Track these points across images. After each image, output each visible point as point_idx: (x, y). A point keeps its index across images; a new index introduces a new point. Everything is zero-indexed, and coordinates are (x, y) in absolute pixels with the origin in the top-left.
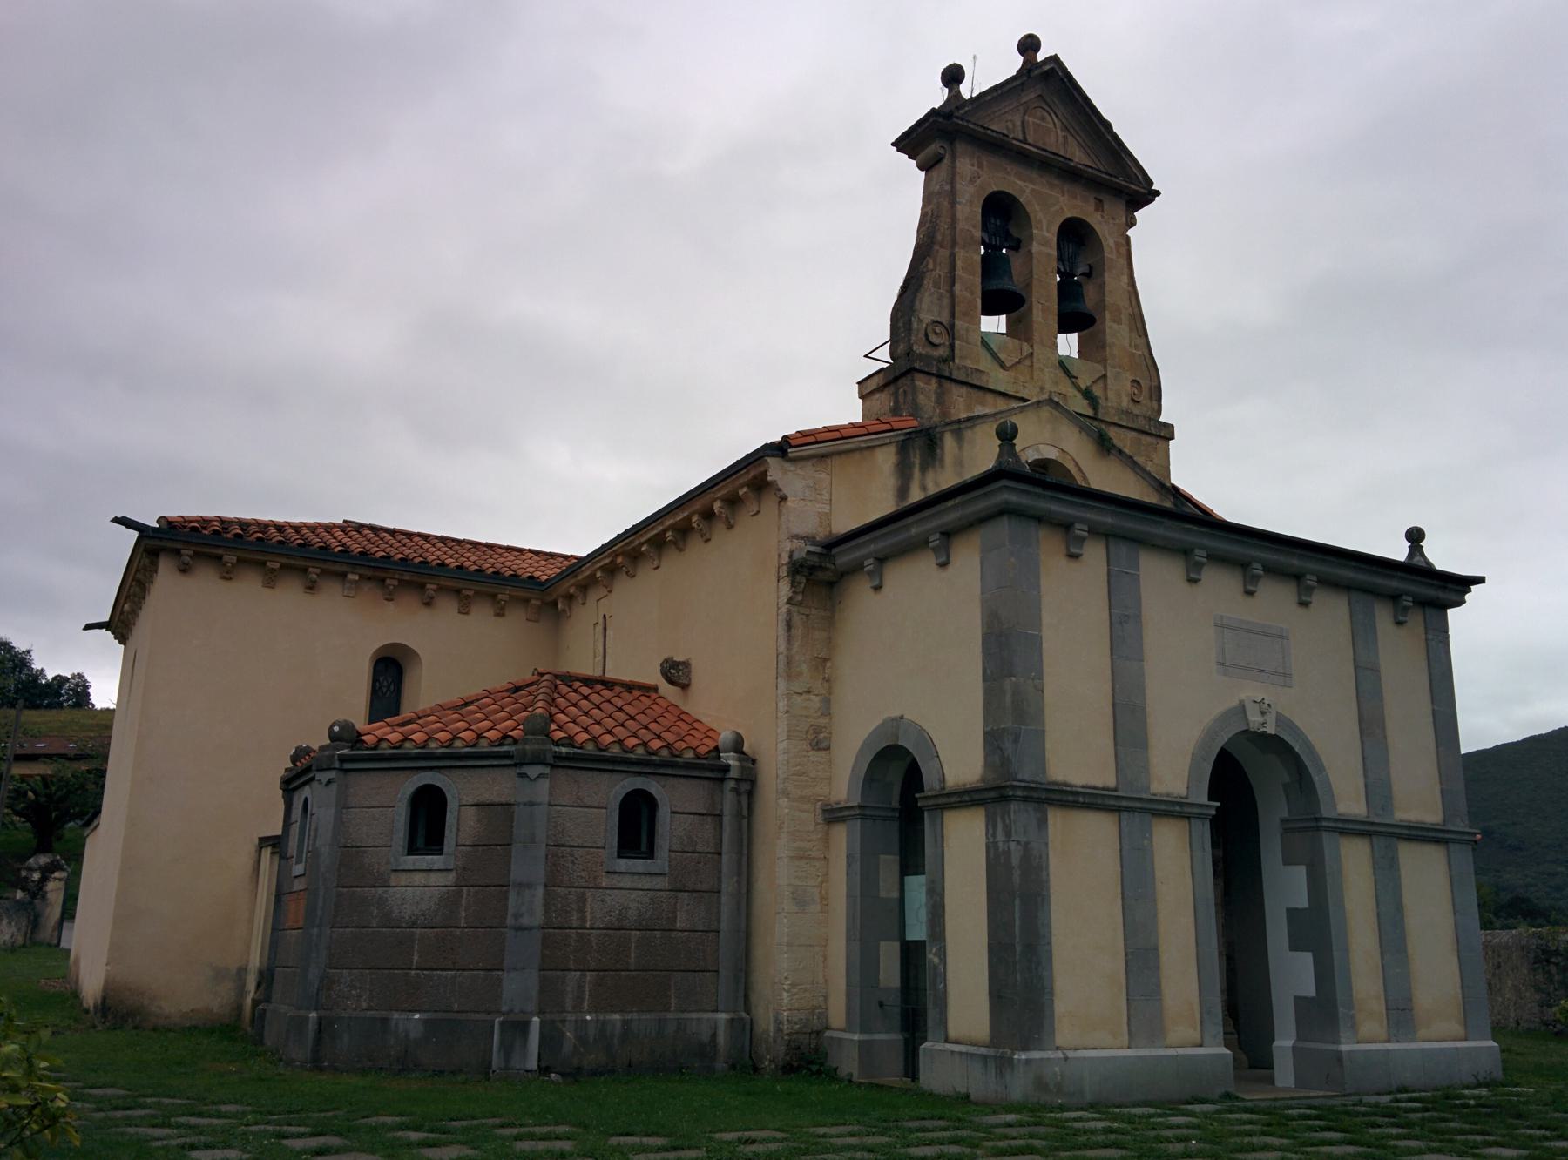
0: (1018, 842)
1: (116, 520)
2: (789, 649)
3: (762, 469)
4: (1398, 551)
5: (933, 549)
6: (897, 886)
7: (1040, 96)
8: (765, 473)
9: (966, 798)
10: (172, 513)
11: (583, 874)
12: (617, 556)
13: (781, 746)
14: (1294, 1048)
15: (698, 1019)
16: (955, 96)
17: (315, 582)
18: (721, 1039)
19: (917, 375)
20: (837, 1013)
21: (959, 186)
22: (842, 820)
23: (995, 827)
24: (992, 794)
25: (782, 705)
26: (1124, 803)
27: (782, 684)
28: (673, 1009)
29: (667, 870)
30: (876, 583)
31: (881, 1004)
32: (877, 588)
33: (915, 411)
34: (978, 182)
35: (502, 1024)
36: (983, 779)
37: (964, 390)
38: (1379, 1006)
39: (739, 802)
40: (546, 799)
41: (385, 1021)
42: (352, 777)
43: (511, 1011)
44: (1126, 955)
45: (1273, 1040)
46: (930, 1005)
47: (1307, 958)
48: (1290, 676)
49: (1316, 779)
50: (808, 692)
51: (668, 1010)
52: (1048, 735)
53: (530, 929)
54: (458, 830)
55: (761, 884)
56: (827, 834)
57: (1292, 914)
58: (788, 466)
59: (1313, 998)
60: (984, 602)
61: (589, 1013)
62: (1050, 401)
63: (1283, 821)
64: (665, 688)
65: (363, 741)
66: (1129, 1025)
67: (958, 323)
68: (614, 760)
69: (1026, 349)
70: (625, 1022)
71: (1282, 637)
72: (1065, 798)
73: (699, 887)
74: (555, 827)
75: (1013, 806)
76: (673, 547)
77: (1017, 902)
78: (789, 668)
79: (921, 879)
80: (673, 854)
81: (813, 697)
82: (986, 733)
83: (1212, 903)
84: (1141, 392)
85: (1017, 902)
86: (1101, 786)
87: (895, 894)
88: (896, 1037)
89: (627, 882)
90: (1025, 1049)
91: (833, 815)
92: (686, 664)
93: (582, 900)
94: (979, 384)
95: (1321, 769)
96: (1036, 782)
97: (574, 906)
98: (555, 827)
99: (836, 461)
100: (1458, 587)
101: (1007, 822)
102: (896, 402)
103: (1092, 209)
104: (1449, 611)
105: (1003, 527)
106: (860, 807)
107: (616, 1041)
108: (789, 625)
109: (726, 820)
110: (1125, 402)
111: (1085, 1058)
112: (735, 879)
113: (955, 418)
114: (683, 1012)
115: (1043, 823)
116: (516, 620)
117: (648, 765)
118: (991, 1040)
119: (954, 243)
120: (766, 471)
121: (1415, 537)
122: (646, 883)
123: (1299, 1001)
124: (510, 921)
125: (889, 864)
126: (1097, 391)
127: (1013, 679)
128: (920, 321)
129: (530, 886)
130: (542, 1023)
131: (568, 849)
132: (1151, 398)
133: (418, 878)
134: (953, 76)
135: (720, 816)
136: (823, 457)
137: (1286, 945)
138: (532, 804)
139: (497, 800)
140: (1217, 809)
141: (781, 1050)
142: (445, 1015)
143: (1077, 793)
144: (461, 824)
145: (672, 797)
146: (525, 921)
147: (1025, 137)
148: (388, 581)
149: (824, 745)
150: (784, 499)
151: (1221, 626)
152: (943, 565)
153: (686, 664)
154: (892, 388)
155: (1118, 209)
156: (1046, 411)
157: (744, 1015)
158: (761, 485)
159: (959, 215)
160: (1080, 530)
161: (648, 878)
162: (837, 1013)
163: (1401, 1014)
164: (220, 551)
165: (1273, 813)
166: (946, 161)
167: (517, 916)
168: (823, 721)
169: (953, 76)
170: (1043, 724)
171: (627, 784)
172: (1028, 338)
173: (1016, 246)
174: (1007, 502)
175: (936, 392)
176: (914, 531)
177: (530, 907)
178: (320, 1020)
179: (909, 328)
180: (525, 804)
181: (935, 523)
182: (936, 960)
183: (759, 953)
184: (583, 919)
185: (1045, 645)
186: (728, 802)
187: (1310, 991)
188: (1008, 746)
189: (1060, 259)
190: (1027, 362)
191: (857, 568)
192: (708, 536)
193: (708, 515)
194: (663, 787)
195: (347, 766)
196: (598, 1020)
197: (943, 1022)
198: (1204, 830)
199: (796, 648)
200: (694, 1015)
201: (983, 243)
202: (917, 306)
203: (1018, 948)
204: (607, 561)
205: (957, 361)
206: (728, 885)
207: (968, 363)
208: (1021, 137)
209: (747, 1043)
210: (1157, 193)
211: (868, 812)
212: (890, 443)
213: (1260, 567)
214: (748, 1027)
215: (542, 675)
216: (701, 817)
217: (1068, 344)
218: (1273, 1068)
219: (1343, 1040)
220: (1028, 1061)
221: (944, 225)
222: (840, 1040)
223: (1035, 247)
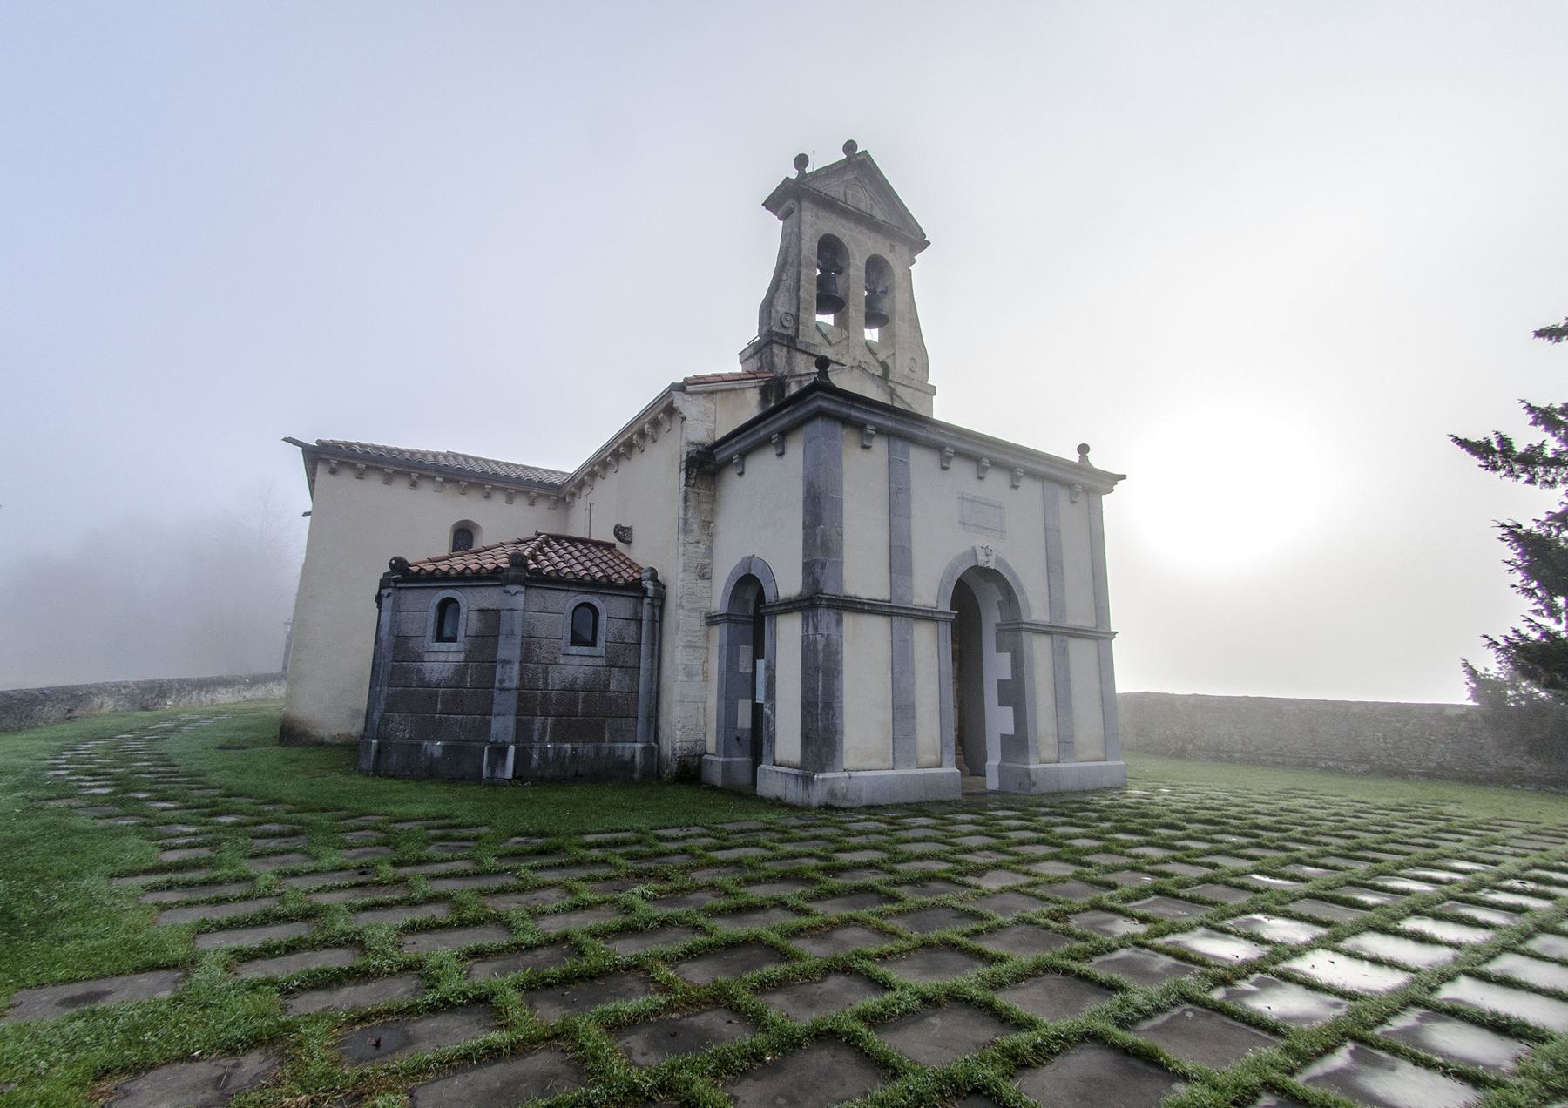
0: (822, 635)
1: (285, 439)
2: (685, 515)
3: (670, 399)
4: (1075, 457)
5: (774, 444)
6: (750, 665)
7: (856, 178)
8: (672, 402)
9: (790, 606)
10: (327, 438)
11: (546, 655)
12: (594, 466)
13: (680, 576)
14: (999, 766)
15: (623, 747)
16: (802, 175)
17: (415, 481)
18: (638, 759)
19: (775, 346)
20: (711, 745)
21: (803, 228)
22: (716, 623)
23: (808, 625)
24: (806, 604)
25: (681, 549)
26: (895, 611)
27: (681, 536)
28: (606, 740)
29: (604, 654)
30: (740, 470)
31: (738, 739)
32: (741, 474)
33: (772, 366)
34: (816, 227)
35: (489, 749)
36: (801, 595)
37: (804, 357)
38: (1053, 741)
39: (654, 613)
40: (521, 607)
41: (419, 745)
42: (403, 592)
43: (496, 741)
44: (893, 710)
45: (986, 760)
46: (765, 741)
47: (1010, 710)
48: (1005, 532)
49: (1019, 598)
50: (698, 542)
51: (603, 741)
52: (845, 565)
53: (509, 690)
54: (467, 626)
55: (666, 663)
56: (708, 633)
57: (1001, 683)
58: (686, 397)
59: (1012, 736)
60: (805, 477)
61: (550, 743)
62: (859, 366)
63: (997, 625)
64: (620, 546)
65: (410, 570)
66: (893, 754)
67: (801, 314)
68: (570, 583)
69: (845, 334)
70: (573, 749)
71: (1000, 507)
72: (855, 606)
73: (625, 665)
74: (528, 625)
75: (820, 611)
76: (624, 457)
77: (821, 674)
78: (685, 527)
79: (763, 661)
80: (608, 644)
81: (701, 546)
82: (804, 564)
83: (951, 676)
84: (916, 365)
85: (821, 674)
86: (880, 599)
87: (749, 670)
88: (747, 759)
89: (577, 661)
90: (823, 771)
91: (712, 620)
92: (630, 529)
93: (546, 672)
94: (814, 353)
95: (1022, 591)
96: (836, 596)
97: (541, 675)
98: (528, 625)
99: (719, 396)
100: (1110, 480)
101: (816, 621)
102: (761, 363)
103: (888, 249)
104: (1103, 496)
105: (819, 426)
106: (726, 614)
107: (567, 760)
108: (686, 500)
109: (644, 623)
110: (906, 371)
111: (863, 777)
112: (650, 660)
113: (798, 373)
114: (613, 742)
115: (839, 622)
116: (542, 508)
117: (593, 585)
118: (802, 762)
119: (799, 264)
120: (673, 401)
121: (1083, 449)
122: (590, 661)
123: (1003, 737)
124: (497, 684)
125: (746, 652)
126: (889, 362)
127: (822, 526)
128: (777, 312)
129: (509, 662)
130: (516, 749)
131: (537, 640)
132: (922, 370)
133: (442, 657)
134: (801, 161)
135: (641, 620)
136: (712, 393)
137: (997, 703)
138: (512, 610)
139: (491, 608)
140: (956, 615)
141: (674, 766)
142: (455, 744)
143: (864, 603)
144: (469, 622)
145: (612, 610)
146: (507, 684)
147: (846, 200)
148: (461, 483)
149: (706, 577)
150: (684, 419)
151: (962, 499)
152: (781, 455)
153: (630, 529)
154: (759, 355)
155: (902, 249)
156: (856, 373)
157: (654, 744)
158: (671, 411)
159: (803, 246)
160: (871, 429)
161: (591, 659)
162: (711, 745)
163: (1066, 745)
164: (355, 462)
165: (992, 619)
166: (795, 214)
167: (501, 681)
168: (707, 561)
169: (801, 161)
170: (842, 558)
171: (574, 599)
172: (847, 328)
173: (840, 272)
174: (819, 407)
175: (786, 357)
176: (762, 433)
177: (511, 676)
178: (379, 745)
179: (770, 317)
180: (508, 610)
181: (772, 428)
182: (769, 712)
183: (664, 707)
184: (546, 684)
185: (844, 505)
186: (646, 613)
187: (1010, 730)
188: (818, 571)
189: (867, 281)
190: (845, 342)
191: (728, 462)
192: (642, 448)
193: (642, 434)
194: (602, 601)
195: (399, 585)
196: (555, 748)
197: (772, 752)
198: (946, 630)
199: (689, 514)
200: (620, 745)
201: (818, 267)
202: (775, 303)
203: (820, 705)
204: (589, 469)
205: (800, 338)
206: (645, 664)
207: (807, 340)
208: (844, 200)
209: (655, 762)
210: (929, 243)
211: (732, 618)
212: (755, 387)
213: (987, 461)
214: (656, 753)
215: (540, 534)
216: (627, 621)
217: (872, 335)
218: (985, 776)
219: (1031, 762)
220: (824, 780)
221: (793, 253)
222: (711, 760)
223: (852, 271)
